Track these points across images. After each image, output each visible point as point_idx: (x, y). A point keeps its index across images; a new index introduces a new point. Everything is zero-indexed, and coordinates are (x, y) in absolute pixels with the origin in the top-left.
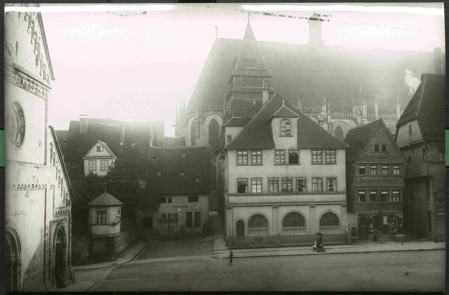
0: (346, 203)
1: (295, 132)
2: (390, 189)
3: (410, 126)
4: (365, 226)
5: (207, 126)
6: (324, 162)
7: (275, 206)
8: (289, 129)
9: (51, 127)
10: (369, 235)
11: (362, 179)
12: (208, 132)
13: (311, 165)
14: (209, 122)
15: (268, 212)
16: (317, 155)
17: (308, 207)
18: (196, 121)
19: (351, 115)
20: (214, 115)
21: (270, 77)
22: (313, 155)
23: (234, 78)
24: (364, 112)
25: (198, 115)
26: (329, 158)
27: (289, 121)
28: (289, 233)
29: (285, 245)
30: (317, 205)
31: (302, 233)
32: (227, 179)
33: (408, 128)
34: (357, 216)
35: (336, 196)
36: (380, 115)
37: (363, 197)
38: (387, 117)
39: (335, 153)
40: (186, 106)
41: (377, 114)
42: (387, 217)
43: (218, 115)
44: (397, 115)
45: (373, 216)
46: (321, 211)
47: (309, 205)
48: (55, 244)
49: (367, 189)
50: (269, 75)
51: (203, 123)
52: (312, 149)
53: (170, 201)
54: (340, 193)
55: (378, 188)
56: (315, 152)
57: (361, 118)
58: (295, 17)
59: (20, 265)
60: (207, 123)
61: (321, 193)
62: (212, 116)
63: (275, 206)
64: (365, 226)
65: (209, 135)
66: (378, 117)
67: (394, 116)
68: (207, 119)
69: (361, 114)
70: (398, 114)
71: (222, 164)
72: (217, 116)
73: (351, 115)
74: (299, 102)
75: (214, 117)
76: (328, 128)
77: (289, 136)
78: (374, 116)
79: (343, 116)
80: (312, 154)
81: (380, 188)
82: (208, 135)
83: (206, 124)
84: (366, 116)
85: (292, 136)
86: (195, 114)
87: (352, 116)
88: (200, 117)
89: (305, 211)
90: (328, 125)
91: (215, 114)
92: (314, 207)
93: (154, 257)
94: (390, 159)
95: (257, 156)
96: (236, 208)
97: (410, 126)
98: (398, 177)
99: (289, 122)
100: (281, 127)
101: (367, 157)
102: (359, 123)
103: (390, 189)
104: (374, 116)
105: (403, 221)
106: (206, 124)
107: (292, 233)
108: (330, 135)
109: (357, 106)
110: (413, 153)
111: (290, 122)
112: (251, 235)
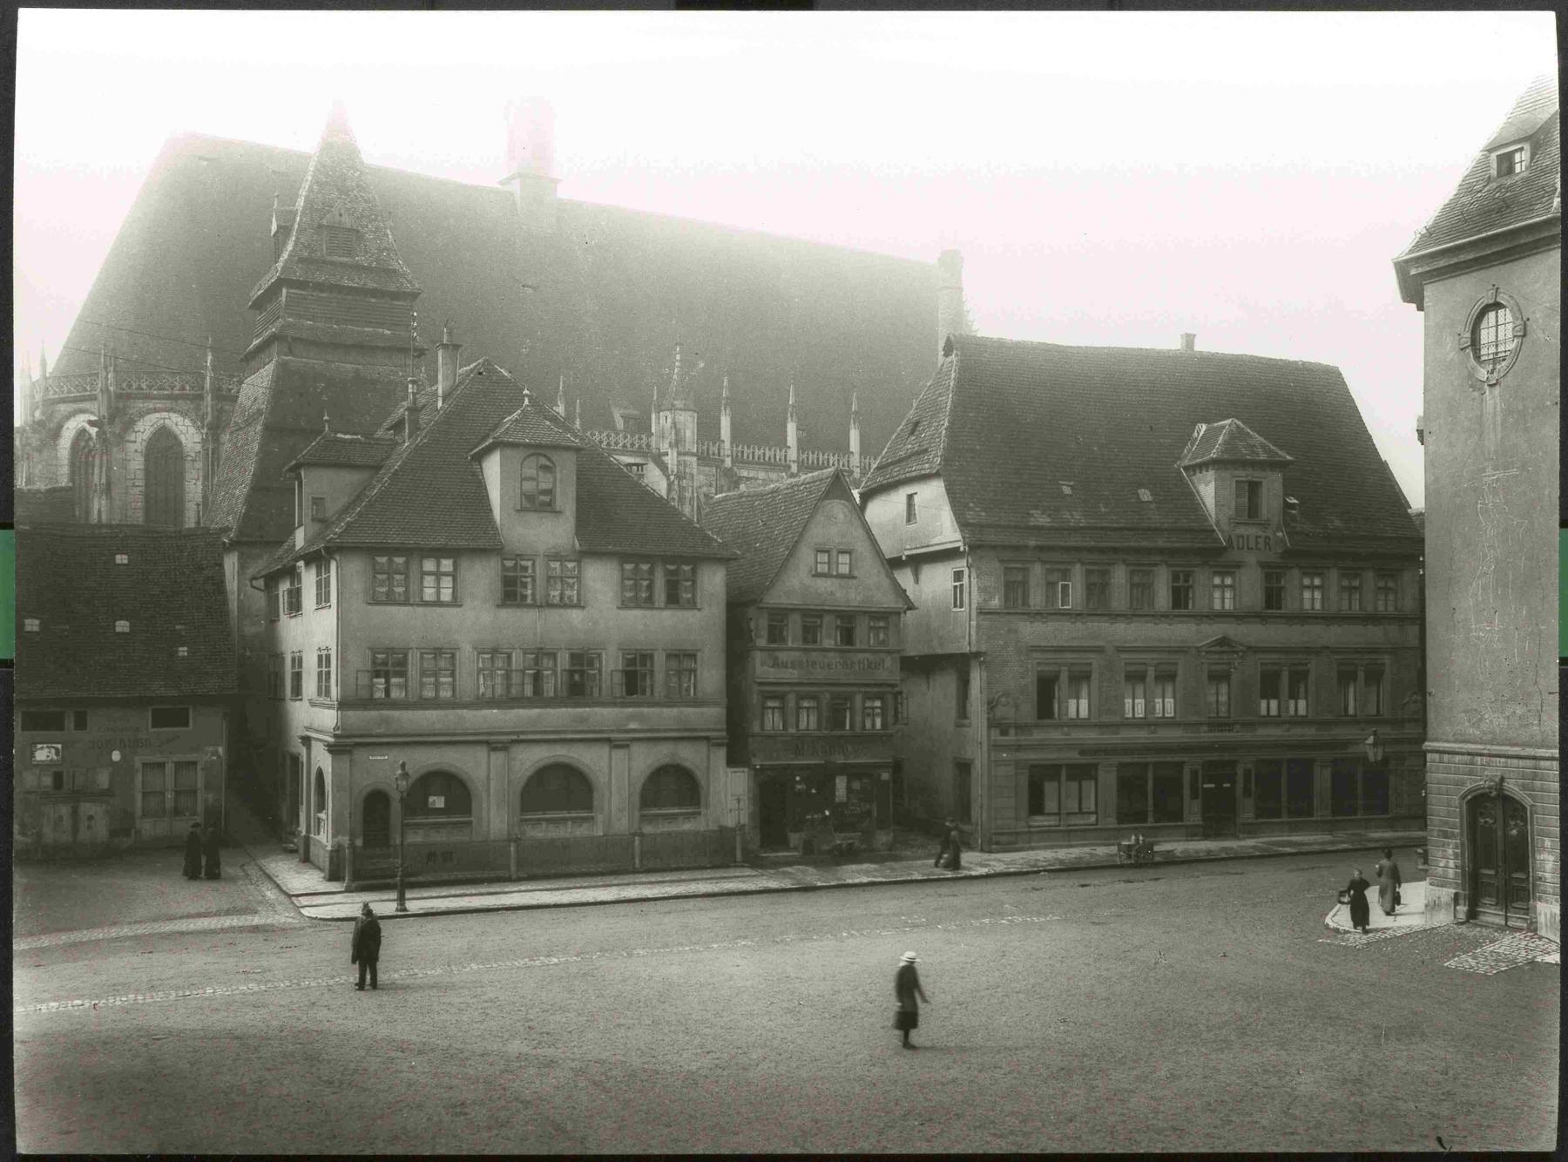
0: (724, 733)
1: (567, 500)
2: (860, 692)
3: (910, 497)
4: (1213, 786)
5: (136, 451)
7: (497, 743)
8: (550, 486)
12: (140, 475)
13: (618, 608)
14: (146, 436)
15: (472, 764)
17: (606, 749)
18: (96, 429)
19: (644, 441)
20: (165, 414)
21: (414, 296)
23: (284, 291)
24: (688, 433)
25: (104, 412)
26: (383, 581)
27: (549, 459)
28: (540, 833)
29: (421, 879)
30: (513, 742)
31: (581, 831)
33: (904, 499)
35: (439, 712)
36: (703, 444)
38: (711, 452)
39: (694, 571)
40: (50, 369)
41: (727, 445)
42: (849, 782)
43: (184, 414)
44: (722, 445)
46: (644, 760)
49: (789, 692)
50: (408, 287)
51: (121, 439)
52: (623, 558)
53: (81, 724)
55: (822, 689)
56: (629, 567)
57: (679, 454)
59: (1080, 858)
60: (139, 440)
61: (509, 701)
62: (157, 415)
63: (497, 743)
64: (1213, 786)
65: (146, 486)
66: (729, 453)
67: (767, 452)
68: (140, 426)
69: (678, 442)
70: (723, 441)
72: (175, 417)
73: (644, 441)
75: (164, 419)
76: (669, 490)
77: (549, 509)
78: (719, 449)
79: (621, 444)
80: (623, 575)
81: (863, 689)
82: (141, 483)
83: (135, 442)
84: (695, 450)
86: (93, 406)
87: (648, 446)
88: (112, 419)
89: (591, 759)
90: (668, 479)
91: (168, 411)
92: (628, 746)
93: (92, 926)
95: (438, 575)
96: (522, 747)
97: (910, 497)
98: (882, 655)
99: (548, 463)
100: (522, 480)
102: (673, 471)
103: (860, 692)
104: (719, 449)
106: (135, 442)
107: (545, 831)
108: (676, 513)
109: (668, 413)
110: (917, 581)
111: (553, 463)
112: (415, 838)
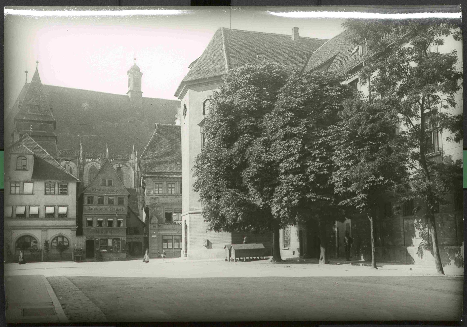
6: (56, 193)
9: (288, 124)
10: (22, 260)
11: (90, 208)
16: (50, 187)
17: (41, 230)
22: (46, 187)
32: (98, 197)
34: (85, 238)
37: (90, 223)
45: (99, 238)
47: (40, 229)
48: (119, 238)
54: (70, 219)
58: (135, 59)
71: (298, 170)
74: (306, 120)
85: (28, 170)
94: (115, 192)
101: (94, 190)
105: (372, 231)
